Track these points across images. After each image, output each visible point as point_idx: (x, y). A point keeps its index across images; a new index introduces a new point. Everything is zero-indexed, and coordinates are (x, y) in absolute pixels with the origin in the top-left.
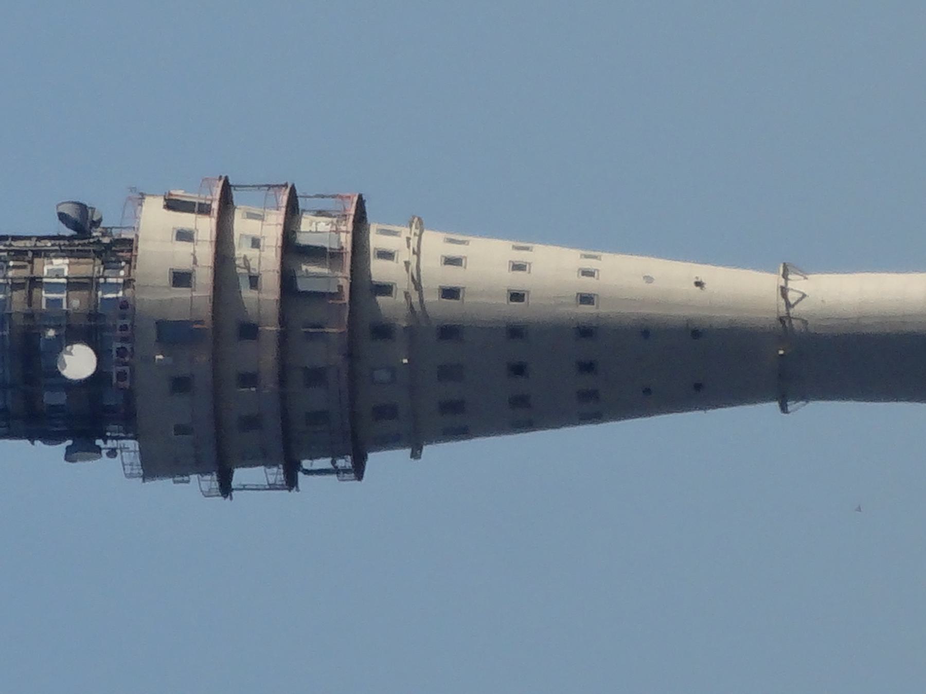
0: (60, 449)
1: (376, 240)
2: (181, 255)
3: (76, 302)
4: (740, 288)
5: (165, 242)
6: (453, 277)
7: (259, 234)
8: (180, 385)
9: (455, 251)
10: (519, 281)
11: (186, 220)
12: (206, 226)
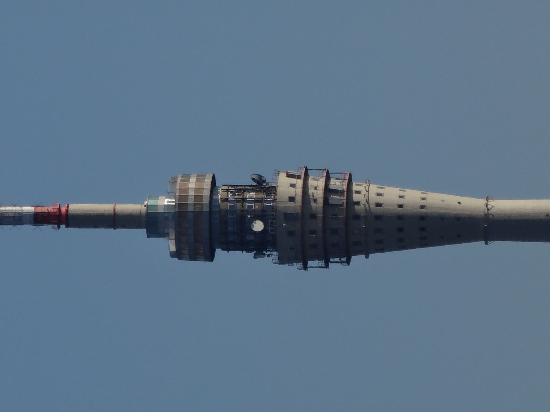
1: (355, 188)
2: (292, 192)
3: (257, 206)
5: (286, 187)
6: (380, 200)
7: (317, 185)
11: (293, 181)
12: (299, 183)
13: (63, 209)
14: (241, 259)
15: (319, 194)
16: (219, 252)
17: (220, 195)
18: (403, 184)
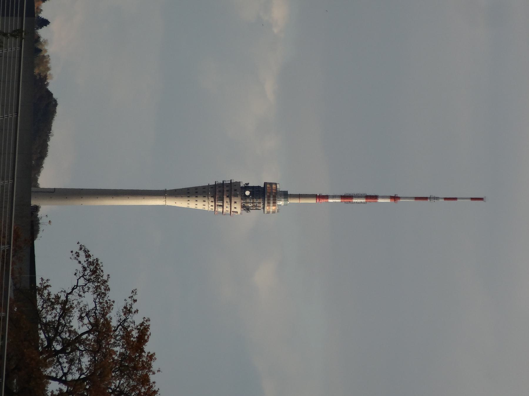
0: (42, 32)
1: (213, 208)
2: (236, 205)
3: (248, 201)
4: (171, 202)
5: (237, 207)
6: (204, 203)
7: (227, 209)
8: (235, 190)
9: (204, 207)
10: (196, 203)
11: (235, 210)
12: (233, 209)
13: (318, 201)
14: (253, 183)
15: (225, 205)
16: (262, 186)
17: (261, 205)
18: (196, 210)
